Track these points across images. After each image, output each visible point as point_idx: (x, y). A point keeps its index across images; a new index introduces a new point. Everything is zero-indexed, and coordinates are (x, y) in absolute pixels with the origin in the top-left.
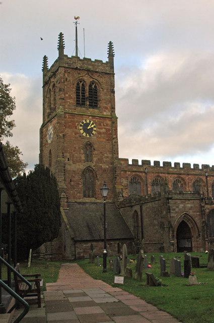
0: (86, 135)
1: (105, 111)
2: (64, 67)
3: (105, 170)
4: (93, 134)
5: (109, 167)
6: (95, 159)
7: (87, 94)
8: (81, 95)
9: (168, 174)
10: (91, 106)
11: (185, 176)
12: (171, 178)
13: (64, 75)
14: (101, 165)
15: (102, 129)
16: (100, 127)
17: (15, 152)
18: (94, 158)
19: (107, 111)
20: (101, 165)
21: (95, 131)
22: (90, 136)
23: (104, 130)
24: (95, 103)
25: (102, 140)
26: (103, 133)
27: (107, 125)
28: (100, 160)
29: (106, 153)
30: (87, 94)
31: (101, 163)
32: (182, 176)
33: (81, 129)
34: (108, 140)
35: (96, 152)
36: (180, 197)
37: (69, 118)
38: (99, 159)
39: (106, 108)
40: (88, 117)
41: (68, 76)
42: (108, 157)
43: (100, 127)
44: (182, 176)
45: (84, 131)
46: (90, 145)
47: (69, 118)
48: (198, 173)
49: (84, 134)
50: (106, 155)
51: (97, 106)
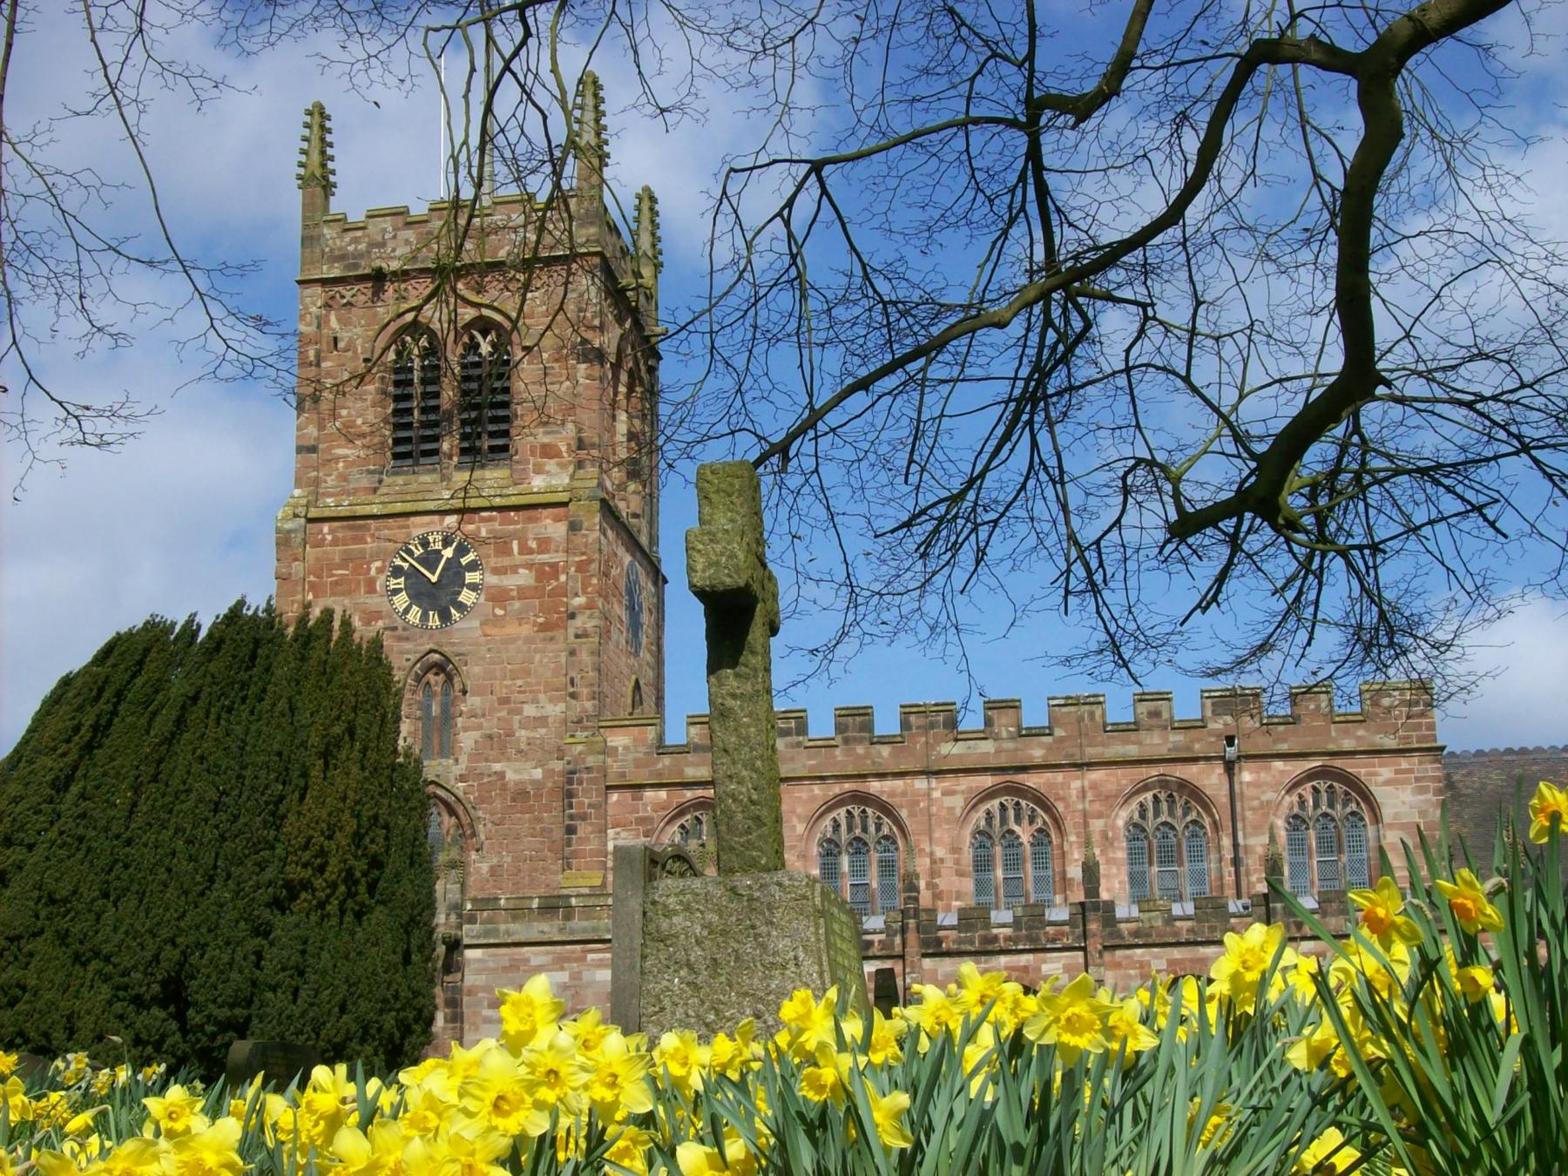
0: (425, 617)
1: (539, 470)
2: (324, 282)
3: (521, 794)
4: (461, 607)
5: (549, 773)
6: (467, 740)
7: (448, 394)
8: (416, 375)
9: (928, 773)
10: (471, 454)
11: (1059, 777)
12: (949, 801)
13: (321, 322)
14: (497, 767)
15: (514, 569)
16: (506, 561)
17: (235, 614)
18: (462, 736)
19: (551, 465)
20: (497, 767)
21: (474, 587)
22: (445, 617)
23: (524, 578)
24: (492, 435)
25: (512, 629)
26: (523, 593)
27: (544, 544)
28: (498, 743)
29: (535, 701)
30: (448, 394)
31: (503, 755)
32: (1032, 780)
33: (396, 592)
34: (543, 628)
35: (473, 701)
36: (547, 928)
37: (335, 542)
38: (490, 737)
39: (548, 451)
40: (1394, 1101)
41: (344, 322)
42: (542, 721)
43: (506, 561)
44: (1032, 780)
45: (415, 597)
46: (439, 668)
47: (335, 542)
48: (1163, 752)
49: (415, 615)
50: (530, 710)
51: (505, 448)
